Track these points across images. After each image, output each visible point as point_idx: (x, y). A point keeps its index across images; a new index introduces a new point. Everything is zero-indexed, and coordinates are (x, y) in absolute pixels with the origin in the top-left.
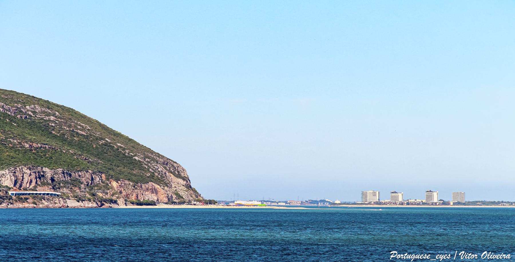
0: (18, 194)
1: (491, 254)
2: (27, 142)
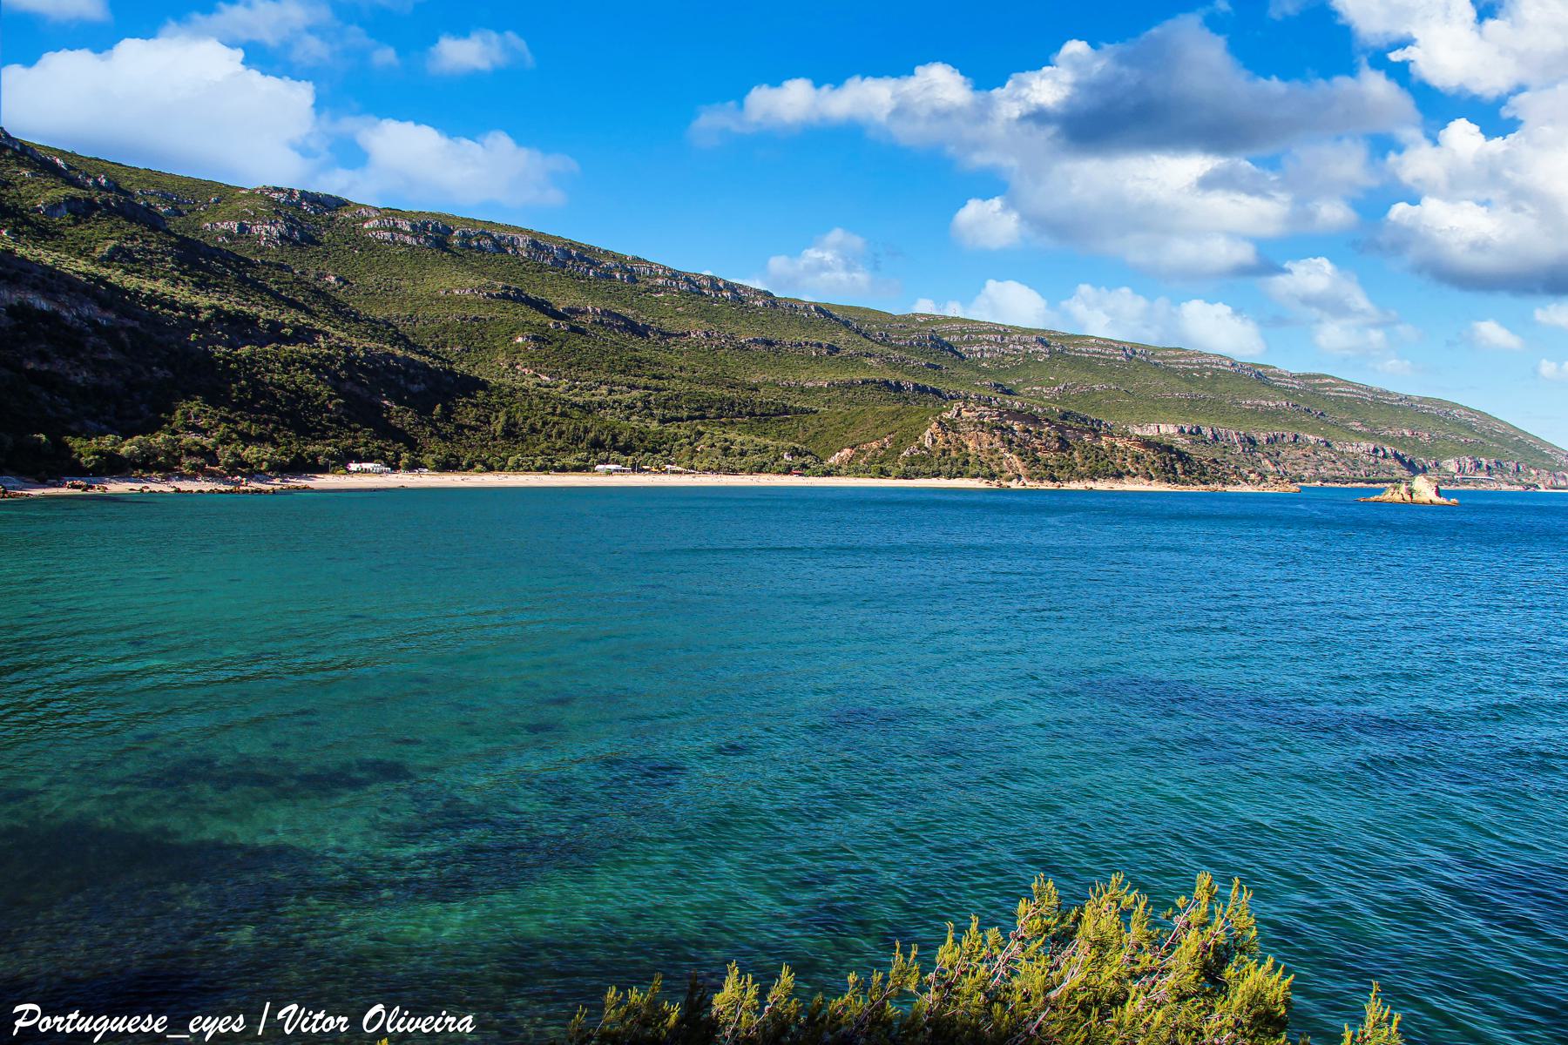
1: (400, 1015)
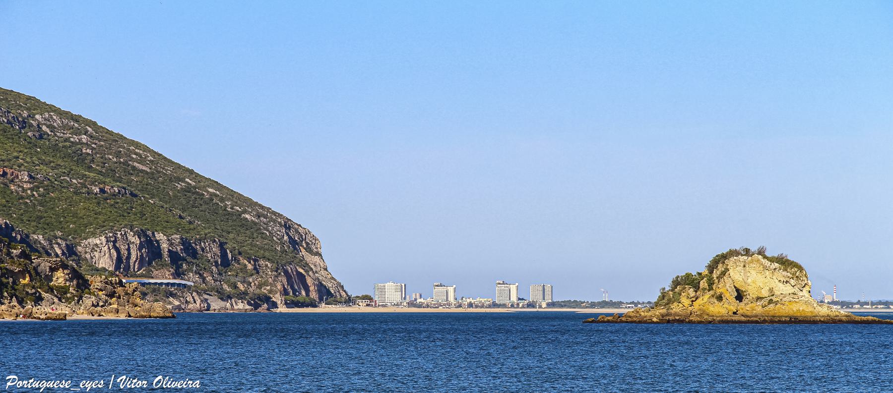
1: (169, 379)
2: (93, 184)
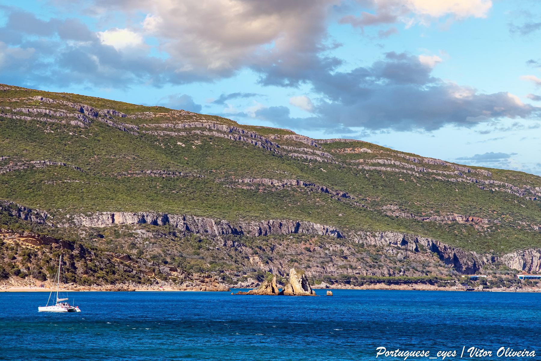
0: (527, 278)
2: (536, 225)
